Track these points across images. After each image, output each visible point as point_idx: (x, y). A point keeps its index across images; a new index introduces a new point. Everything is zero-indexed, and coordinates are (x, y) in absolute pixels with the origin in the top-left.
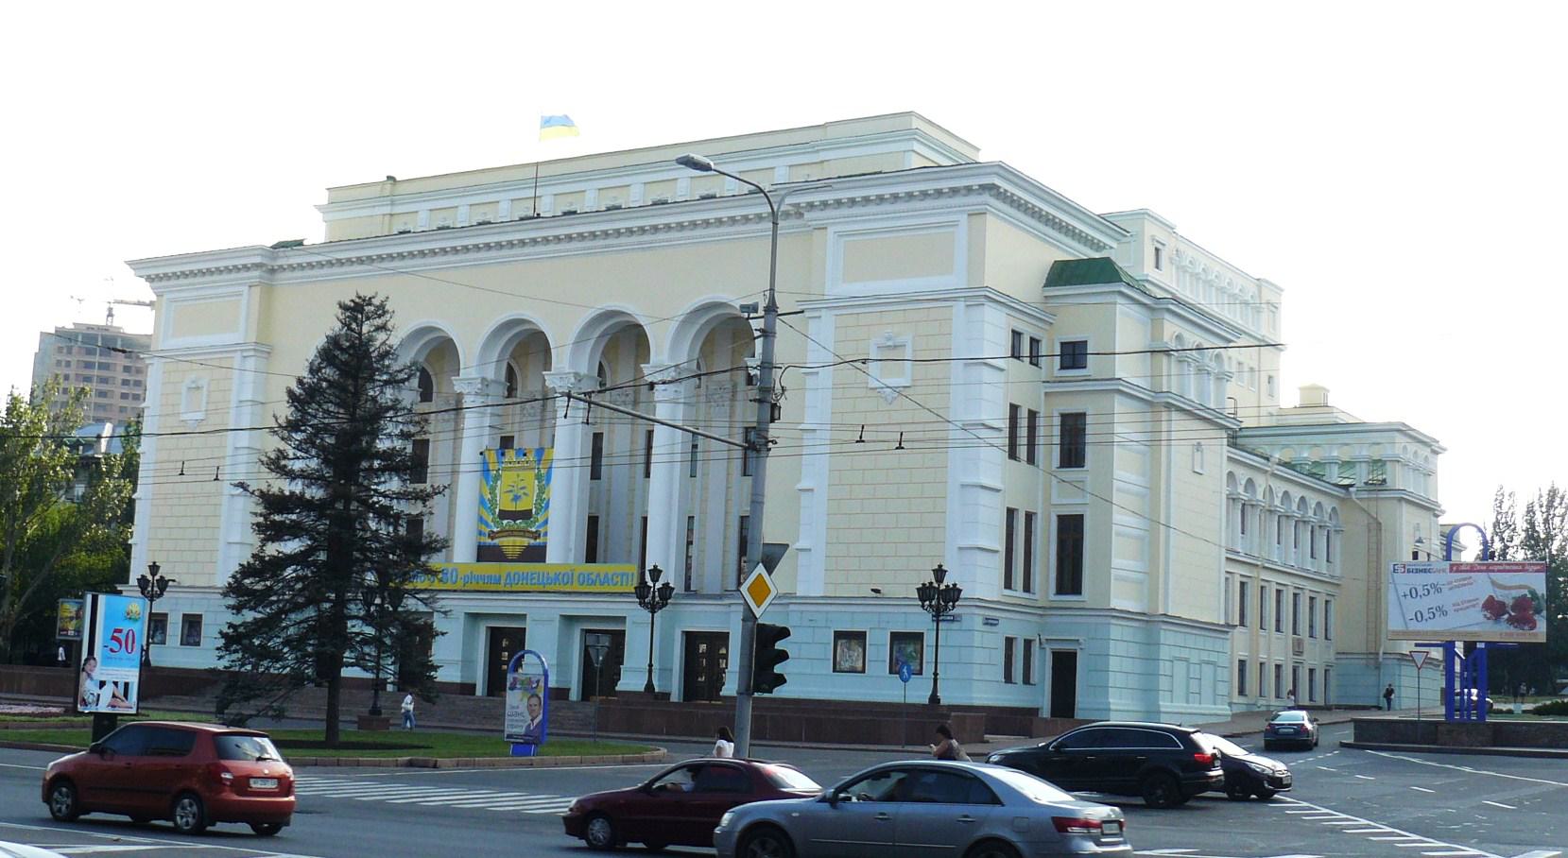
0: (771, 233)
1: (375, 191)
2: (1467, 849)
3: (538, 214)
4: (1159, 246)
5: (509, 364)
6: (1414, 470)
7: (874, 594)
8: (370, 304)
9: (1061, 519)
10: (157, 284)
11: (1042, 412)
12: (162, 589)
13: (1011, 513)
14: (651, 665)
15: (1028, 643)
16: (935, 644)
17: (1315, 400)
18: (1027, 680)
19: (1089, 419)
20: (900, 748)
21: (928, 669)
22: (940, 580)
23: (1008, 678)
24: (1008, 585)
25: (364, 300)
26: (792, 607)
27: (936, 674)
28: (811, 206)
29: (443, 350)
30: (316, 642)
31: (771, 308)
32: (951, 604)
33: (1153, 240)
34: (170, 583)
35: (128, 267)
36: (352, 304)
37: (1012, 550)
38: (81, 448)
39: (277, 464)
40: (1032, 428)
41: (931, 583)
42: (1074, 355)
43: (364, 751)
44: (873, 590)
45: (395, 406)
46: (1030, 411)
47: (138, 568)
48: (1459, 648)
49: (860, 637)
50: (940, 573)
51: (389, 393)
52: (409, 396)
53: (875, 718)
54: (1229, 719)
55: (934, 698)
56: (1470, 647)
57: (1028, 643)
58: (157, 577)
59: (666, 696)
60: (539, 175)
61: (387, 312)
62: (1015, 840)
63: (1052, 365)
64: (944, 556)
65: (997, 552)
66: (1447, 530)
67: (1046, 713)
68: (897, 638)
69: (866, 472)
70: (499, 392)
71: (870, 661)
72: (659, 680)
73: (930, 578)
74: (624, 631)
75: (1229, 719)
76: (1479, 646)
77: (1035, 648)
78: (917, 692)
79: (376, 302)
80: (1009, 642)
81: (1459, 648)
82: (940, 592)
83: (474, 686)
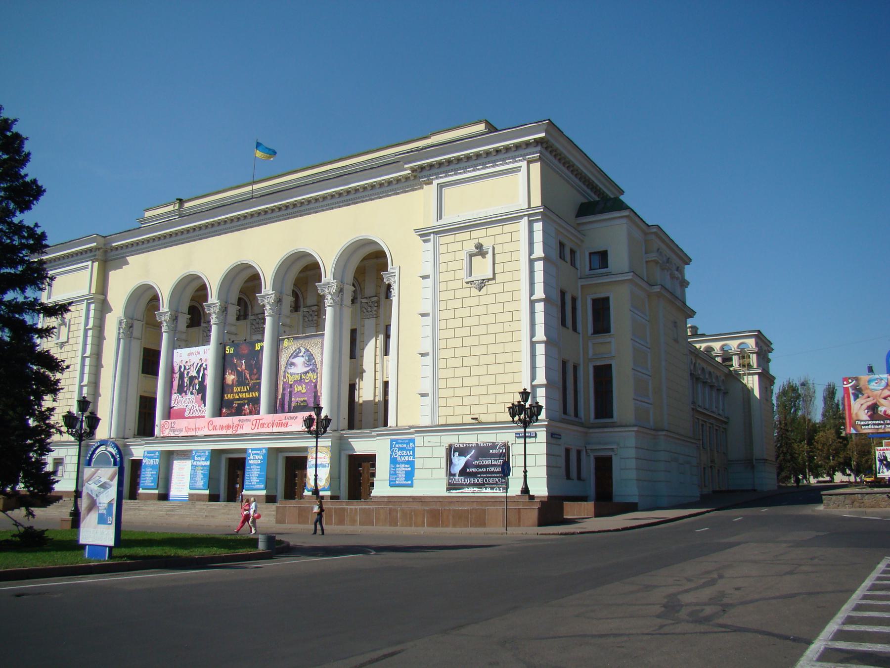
6: (704, 382)
7: (474, 421)
9: (597, 369)
15: (579, 452)
23: (568, 476)
37: (577, 377)
41: (519, 402)
44: (472, 419)
54: (699, 499)
57: (579, 452)
63: (583, 261)
69: (464, 299)
73: (518, 398)
75: (699, 499)
80: (568, 451)
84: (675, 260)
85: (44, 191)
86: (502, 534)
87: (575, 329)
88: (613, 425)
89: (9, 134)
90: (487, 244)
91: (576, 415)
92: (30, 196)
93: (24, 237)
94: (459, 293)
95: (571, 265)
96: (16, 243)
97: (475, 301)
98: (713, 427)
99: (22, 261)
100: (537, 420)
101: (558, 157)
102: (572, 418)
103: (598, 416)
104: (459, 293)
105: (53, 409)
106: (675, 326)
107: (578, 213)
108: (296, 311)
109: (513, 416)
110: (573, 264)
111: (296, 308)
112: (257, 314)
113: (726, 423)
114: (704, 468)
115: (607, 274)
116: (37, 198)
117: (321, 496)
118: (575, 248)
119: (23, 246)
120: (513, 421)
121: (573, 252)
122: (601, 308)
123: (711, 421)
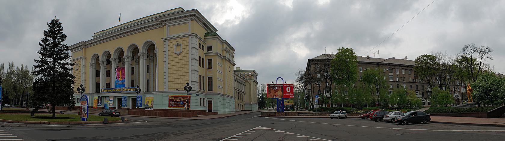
13: (200, 76)
18: (204, 106)
22: (188, 86)
24: (200, 89)
26: (163, 93)
28: (163, 21)
43: (45, 119)
46: (203, 58)
53: (416, 111)
63: (206, 49)
65: (198, 82)
67: (207, 111)
71: (168, 36)
82: (188, 88)
83: (116, 108)
84: (231, 51)
85: (66, 37)
87: (203, 67)
88: (212, 93)
89: (58, 23)
90: (180, 43)
92: (64, 38)
93: (64, 48)
94: (173, 56)
96: (63, 49)
97: (177, 59)
99: (64, 53)
100: (191, 91)
101: (200, 21)
102: (202, 90)
104: (173, 56)
105: (74, 87)
108: (133, 60)
109: (185, 89)
111: (133, 59)
115: (212, 53)
116: (66, 38)
118: (204, 45)
119: (64, 50)
120: (185, 91)
121: (203, 46)
122: (210, 62)
123: (241, 92)
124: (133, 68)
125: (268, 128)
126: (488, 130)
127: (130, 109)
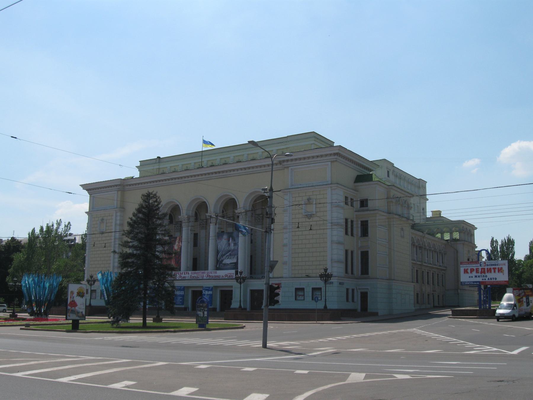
0: (273, 169)
1: (154, 161)
2: (470, 343)
3: (203, 167)
4: (389, 170)
5: (195, 212)
7: (306, 277)
8: (152, 194)
10: (89, 191)
11: (355, 220)
12: (94, 283)
13: (346, 251)
14: (240, 300)
15: (353, 290)
16: (326, 292)
17: (437, 214)
18: (353, 301)
19: (369, 222)
20: (315, 322)
21: (323, 299)
23: (347, 300)
25: (150, 193)
27: (326, 300)
29: (176, 209)
30: (487, 308)
31: (271, 190)
32: (329, 279)
33: (387, 168)
34: (97, 281)
35: (80, 187)
36: (146, 194)
38: (70, 242)
39: (125, 244)
40: (352, 226)
42: (364, 203)
45: (160, 225)
47: (87, 277)
48: (482, 287)
49: (302, 289)
50: (326, 270)
51: (159, 222)
52: (166, 221)
55: (325, 307)
56: (486, 287)
57: (353, 290)
58: (92, 279)
59: (245, 309)
60: (203, 155)
61: (157, 196)
62: (355, 233)
63: (357, 205)
64: (327, 265)
66: (477, 252)
67: (359, 310)
68: (314, 289)
70: (192, 219)
72: (243, 304)
74: (232, 290)
76: (488, 286)
77: (355, 291)
78: (320, 305)
79: (154, 193)
80: (347, 290)
81: (482, 287)
86: (189, 242)
91: (352, 273)
95: (351, 206)
98: (435, 273)
103: (362, 274)
106: (402, 230)
107: (355, 181)
110: (352, 205)
112: (203, 220)
113: (444, 270)
114: (443, 296)
115: (368, 210)
117: (509, 280)
122: (365, 226)
124: (196, 236)
125: (19, 374)
126: (190, 322)
127: (248, 310)
